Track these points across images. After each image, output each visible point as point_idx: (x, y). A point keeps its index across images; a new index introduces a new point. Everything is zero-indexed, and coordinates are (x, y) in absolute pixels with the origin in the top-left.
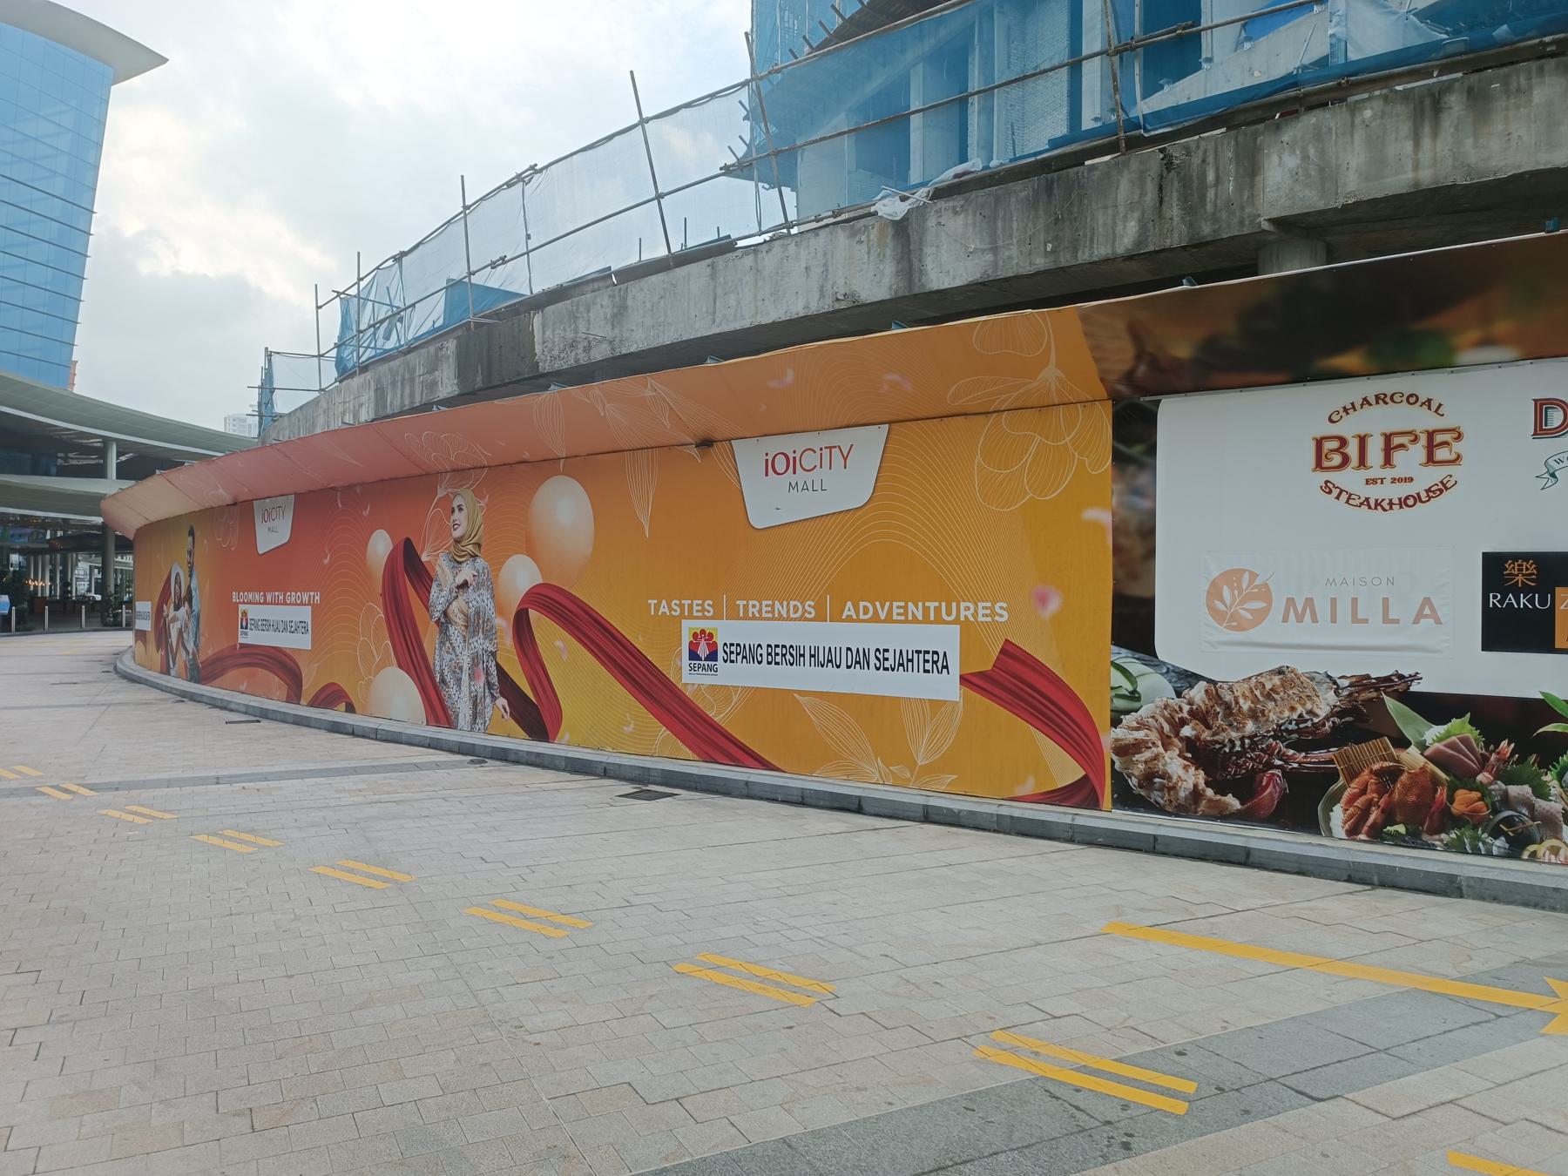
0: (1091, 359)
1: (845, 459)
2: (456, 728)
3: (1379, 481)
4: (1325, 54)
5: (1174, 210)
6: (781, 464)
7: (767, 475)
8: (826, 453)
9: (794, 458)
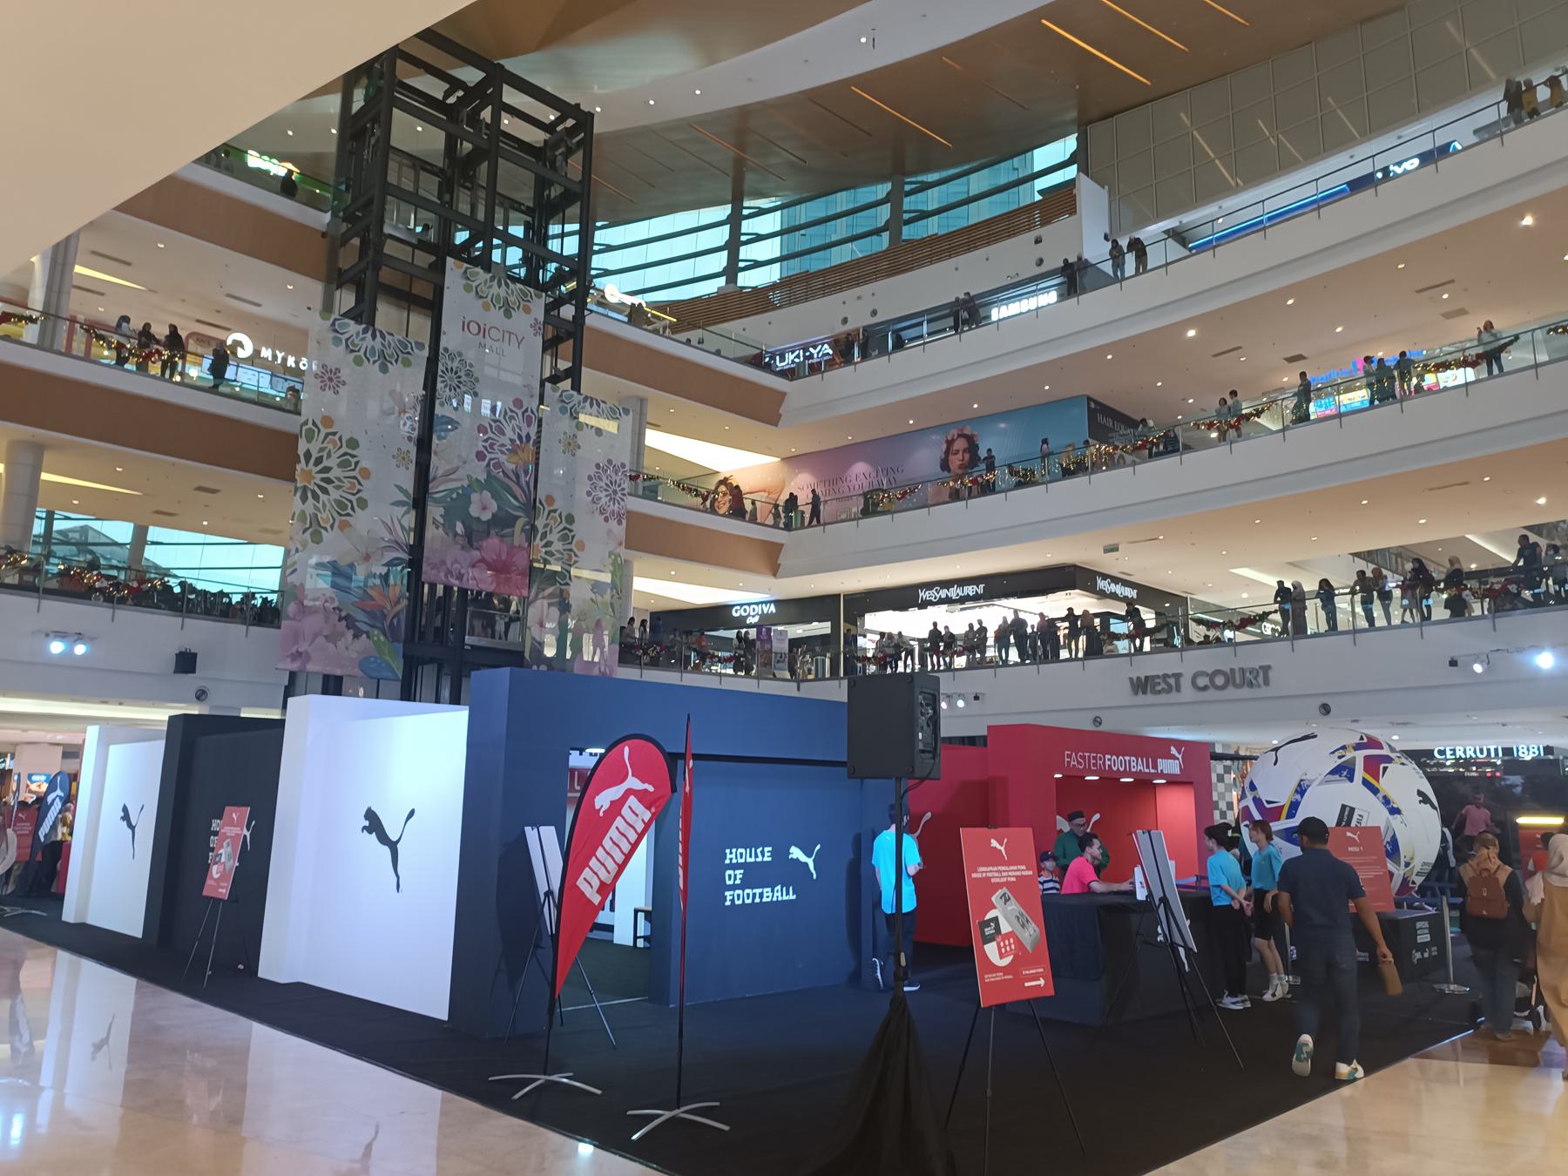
1: (519, 344)
7: (463, 329)
8: (507, 335)
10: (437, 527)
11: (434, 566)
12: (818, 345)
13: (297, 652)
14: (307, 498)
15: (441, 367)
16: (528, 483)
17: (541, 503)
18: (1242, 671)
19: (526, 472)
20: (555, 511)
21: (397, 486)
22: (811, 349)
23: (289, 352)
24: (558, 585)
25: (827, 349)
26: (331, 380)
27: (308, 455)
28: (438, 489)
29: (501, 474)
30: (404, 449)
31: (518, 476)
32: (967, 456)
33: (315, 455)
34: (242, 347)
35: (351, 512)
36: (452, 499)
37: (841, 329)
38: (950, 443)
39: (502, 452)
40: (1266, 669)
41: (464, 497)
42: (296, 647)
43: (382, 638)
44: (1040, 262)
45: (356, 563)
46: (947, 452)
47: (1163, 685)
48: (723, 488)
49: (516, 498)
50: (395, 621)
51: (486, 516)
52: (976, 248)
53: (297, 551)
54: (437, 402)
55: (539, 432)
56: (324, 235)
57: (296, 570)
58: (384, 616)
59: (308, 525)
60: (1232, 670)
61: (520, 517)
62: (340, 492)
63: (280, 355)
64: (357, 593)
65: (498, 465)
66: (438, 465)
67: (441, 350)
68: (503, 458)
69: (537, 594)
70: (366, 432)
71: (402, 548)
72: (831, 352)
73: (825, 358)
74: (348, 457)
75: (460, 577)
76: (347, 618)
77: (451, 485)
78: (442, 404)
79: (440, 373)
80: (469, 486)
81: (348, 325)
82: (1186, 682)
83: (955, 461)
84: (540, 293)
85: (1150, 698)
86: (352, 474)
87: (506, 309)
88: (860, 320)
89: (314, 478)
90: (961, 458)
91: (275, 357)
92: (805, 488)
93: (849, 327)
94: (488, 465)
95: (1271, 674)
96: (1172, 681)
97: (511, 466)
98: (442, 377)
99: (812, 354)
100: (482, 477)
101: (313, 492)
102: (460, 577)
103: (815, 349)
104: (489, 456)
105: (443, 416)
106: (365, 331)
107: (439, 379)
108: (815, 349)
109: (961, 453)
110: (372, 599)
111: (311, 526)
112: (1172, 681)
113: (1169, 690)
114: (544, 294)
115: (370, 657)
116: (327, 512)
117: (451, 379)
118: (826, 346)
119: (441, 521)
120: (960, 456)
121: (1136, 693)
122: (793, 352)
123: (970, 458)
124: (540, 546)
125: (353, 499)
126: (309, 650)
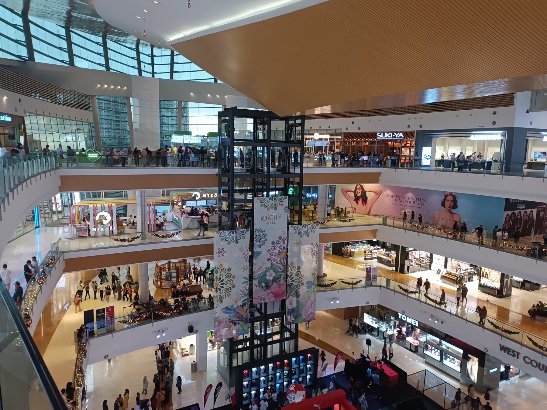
6: (265, 218)
10: (256, 287)
11: (256, 299)
15: (255, 236)
16: (284, 263)
17: (289, 266)
19: (284, 260)
20: (294, 267)
21: (243, 277)
22: (395, 134)
23: (210, 194)
25: (401, 135)
27: (217, 278)
28: (256, 275)
30: (245, 265)
31: (281, 262)
32: (452, 204)
33: (219, 277)
34: (197, 196)
35: (231, 274)
36: (261, 276)
37: (407, 130)
39: (276, 256)
41: (264, 274)
43: (243, 323)
44: (494, 123)
46: (445, 199)
47: (512, 353)
49: (281, 269)
51: (271, 278)
53: (216, 307)
54: (254, 247)
55: (287, 245)
56: (217, 175)
58: (243, 317)
61: (282, 275)
63: (208, 195)
65: (275, 260)
67: (254, 230)
68: (276, 258)
71: (246, 296)
72: (403, 137)
73: (400, 139)
75: (264, 299)
76: (232, 321)
77: (260, 272)
79: (254, 238)
80: (266, 270)
83: (447, 204)
87: (275, 207)
88: (415, 128)
89: (218, 283)
90: (450, 203)
91: (207, 195)
92: (389, 196)
94: (272, 262)
96: (516, 354)
98: (255, 239)
100: (270, 266)
101: (219, 289)
102: (264, 299)
104: (272, 259)
106: (230, 232)
107: (254, 240)
109: (450, 201)
111: (219, 299)
112: (516, 354)
113: (514, 356)
116: (224, 293)
117: (258, 238)
118: (401, 134)
119: (258, 284)
120: (449, 202)
121: (501, 350)
122: (388, 133)
123: (454, 204)
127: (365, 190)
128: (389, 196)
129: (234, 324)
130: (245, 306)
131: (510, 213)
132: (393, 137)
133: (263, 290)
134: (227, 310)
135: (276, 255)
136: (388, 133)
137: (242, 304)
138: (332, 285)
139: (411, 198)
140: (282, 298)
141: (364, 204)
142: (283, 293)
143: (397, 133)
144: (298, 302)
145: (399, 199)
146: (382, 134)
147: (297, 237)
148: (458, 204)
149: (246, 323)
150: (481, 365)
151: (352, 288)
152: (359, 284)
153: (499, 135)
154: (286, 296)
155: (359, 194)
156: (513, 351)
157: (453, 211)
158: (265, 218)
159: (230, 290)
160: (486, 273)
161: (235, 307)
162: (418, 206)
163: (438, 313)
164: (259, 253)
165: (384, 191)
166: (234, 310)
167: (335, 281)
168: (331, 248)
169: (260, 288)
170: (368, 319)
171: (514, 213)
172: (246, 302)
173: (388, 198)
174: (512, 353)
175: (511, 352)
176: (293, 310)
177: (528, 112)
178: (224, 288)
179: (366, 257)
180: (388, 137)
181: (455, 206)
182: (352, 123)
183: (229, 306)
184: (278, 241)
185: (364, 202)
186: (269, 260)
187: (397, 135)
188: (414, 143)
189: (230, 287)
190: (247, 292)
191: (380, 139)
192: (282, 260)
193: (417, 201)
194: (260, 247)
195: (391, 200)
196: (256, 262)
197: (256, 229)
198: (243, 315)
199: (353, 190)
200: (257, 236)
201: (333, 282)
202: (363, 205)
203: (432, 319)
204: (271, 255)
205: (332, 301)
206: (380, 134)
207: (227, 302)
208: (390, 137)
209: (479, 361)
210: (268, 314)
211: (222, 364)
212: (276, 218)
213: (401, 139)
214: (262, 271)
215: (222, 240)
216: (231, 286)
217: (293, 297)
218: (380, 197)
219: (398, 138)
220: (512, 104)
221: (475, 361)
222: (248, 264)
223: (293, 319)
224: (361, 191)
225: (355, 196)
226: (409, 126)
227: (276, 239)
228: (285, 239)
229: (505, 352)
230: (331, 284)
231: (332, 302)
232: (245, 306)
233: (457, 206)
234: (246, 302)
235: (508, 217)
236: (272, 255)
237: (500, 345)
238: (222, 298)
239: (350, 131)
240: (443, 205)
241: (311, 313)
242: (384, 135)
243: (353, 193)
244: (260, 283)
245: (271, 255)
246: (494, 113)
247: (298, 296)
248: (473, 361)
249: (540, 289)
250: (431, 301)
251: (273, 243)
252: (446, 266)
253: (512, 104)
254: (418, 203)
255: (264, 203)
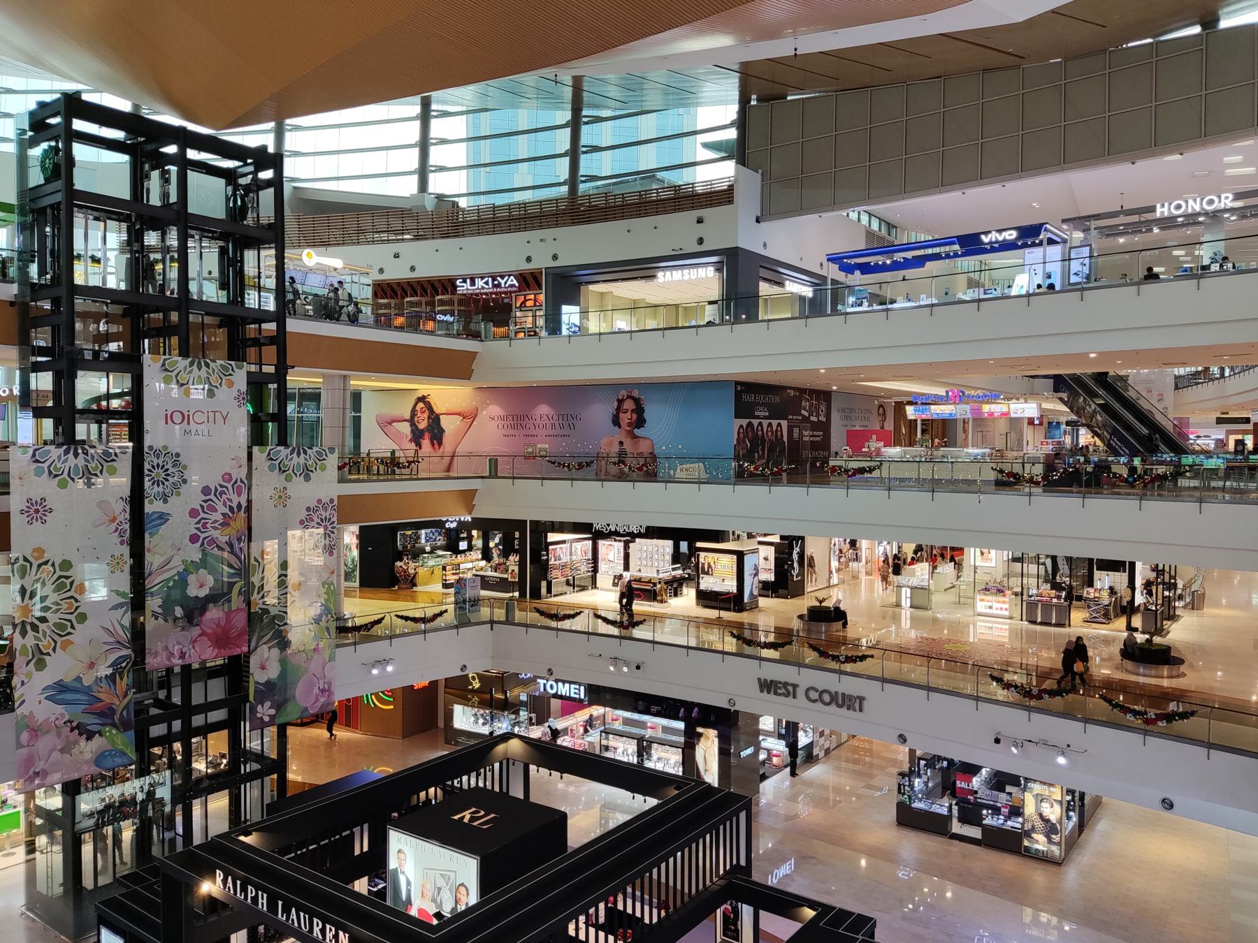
0: (76, 776)
1: (225, 419)
2: (554, 274)
3: (503, 468)
4: (852, 910)
5: (583, 179)
6: (178, 418)
7: (167, 423)
8: (211, 415)
9: (188, 415)
10: (156, 618)
12: (506, 276)
13: (35, 772)
14: (27, 632)
15: (147, 466)
18: (843, 694)
19: (239, 540)
22: (499, 278)
24: (277, 627)
26: (37, 511)
28: (154, 582)
29: (216, 549)
32: (635, 416)
37: (525, 266)
38: (620, 402)
39: (215, 528)
40: (861, 699)
41: (182, 581)
42: (32, 769)
43: (114, 732)
44: (701, 241)
45: (81, 675)
46: (618, 409)
47: (783, 691)
48: (421, 405)
50: (125, 713)
52: (647, 215)
54: (146, 501)
56: (12, 304)
57: (24, 701)
58: (113, 711)
59: (31, 657)
60: (836, 693)
61: (235, 583)
62: (59, 615)
64: (85, 700)
65: (213, 541)
66: (152, 560)
67: (146, 449)
68: (215, 534)
69: (257, 643)
70: (78, 550)
72: (517, 285)
74: (63, 579)
76: (78, 727)
78: (151, 502)
79: (146, 472)
81: (49, 451)
82: (801, 692)
83: (625, 418)
84: (241, 363)
85: (772, 697)
86: (68, 594)
88: (542, 262)
92: (496, 419)
93: (533, 266)
94: (203, 544)
95: (865, 703)
96: (790, 688)
97: (223, 539)
99: (500, 284)
100: (196, 556)
103: (503, 279)
104: (203, 536)
105: (154, 513)
107: (147, 479)
108: (503, 279)
109: (629, 412)
110: (100, 700)
112: (790, 688)
113: (787, 695)
114: (245, 363)
115: (105, 752)
116: (48, 638)
117: (158, 475)
118: (512, 277)
119: (160, 611)
121: (762, 691)
124: (259, 606)
125: (72, 617)
126: (45, 768)
127: (437, 411)
128: (496, 419)
129: (84, 736)
130: (121, 679)
131: (744, 422)
132: (494, 286)
133: (176, 627)
134: (59, 692)
135: (216, 525)
136: (482, 278)
137: (110, 671)
138: (372, 627)
139: (545, 417)
140: (237, 651)
141: (436, 446)
142: (239, 635)
143: (503, 277)
144: (283, 662)
145: (519, 422)
146: (468, 281)
147: (276, 479)
148: (646, 415)
149: (125, 730)
150: (725, 742)
151: (425, 632)
152: (440, 622)
153: (711, 270)
154: (249, 646)
155: (422, 425)
156: (786, 684)
157: (637, 432)
158: (178, 418)
159: (69, 630)
160: (709, 564)
161: (86, 683)
162: (562, 432)
163: (627, 649)
164: (163, 518)
165: (484, 409)
166: (87, 691)
167: (380, 616)
168: (357, 573)
169: (166, 621)
170: (465, 718)
171: (750, 424)
172: (123, 665)
173: (495, 423)
174: (783, 691)
175: (780, 688)
176: (270, 685)
177: (758, 221)
178: (50, 624)
179: (446, 580)
180: (483, 288)
181: (640, 422)
182: (395, 257)
183: (68, 679)
184: (221, 486)
185: (435, 442)
186: (194, 539)
187: (503, 282)
188: (542, 297)
189: (70, 621)
190: (125, 636)
191: (465, 292)
192: (236, 543)
193: (561, 422)
194: (165, 501)
195: (501, 427)
196: (152, 546)
197: (151, 448)
198: (115, 707)
199: (407, 415)
200: (153, 467)
201: (376, 618)
202: (434, 449)
203: (615, 666)
204: (200, 526)
205: (373, 666)
206: (465, 281)
207: (60, 667)
208: (487, 287)
209: (720, 737)
210: (193, 704)
211: (41, 887)
212: (211, 419)
213: (514, 289)
214: (174, 572)
215: (39, 473)
216: (72, 617)
217: (270, 648)
218: (475, 423)
219: (505, 287)
220: (731, 201)
221: (711, 738)
222: (126, 550)
223: (273, 712)
224: (426, 415)
225: (412, 431)
226: (529, 259)
227: (214, 481)
228: (242, 481)
229: (769, 693)
230: (371, 623)
231: (375, 672)
232: (121, 679)
233: (645, 421)
234: (123, 665)
235: (741, 431)
236: (204, 526)
237: (759, 679)
238: (42, 653)
239: (390, 275)
240: (616, 422)
241: (323, 691)
242: (473, 283)
243: (407, 425)
244: (167, 607)
245: (200, 526)
246: (700, 221)
247: (284, 644)
248: (708, 738)
249: (804, 594)
250: (609, 626)
251: (206, 490)
252: (627, 568)
253: (731, 201)
254: (562, 427)
255: (174, 374)
